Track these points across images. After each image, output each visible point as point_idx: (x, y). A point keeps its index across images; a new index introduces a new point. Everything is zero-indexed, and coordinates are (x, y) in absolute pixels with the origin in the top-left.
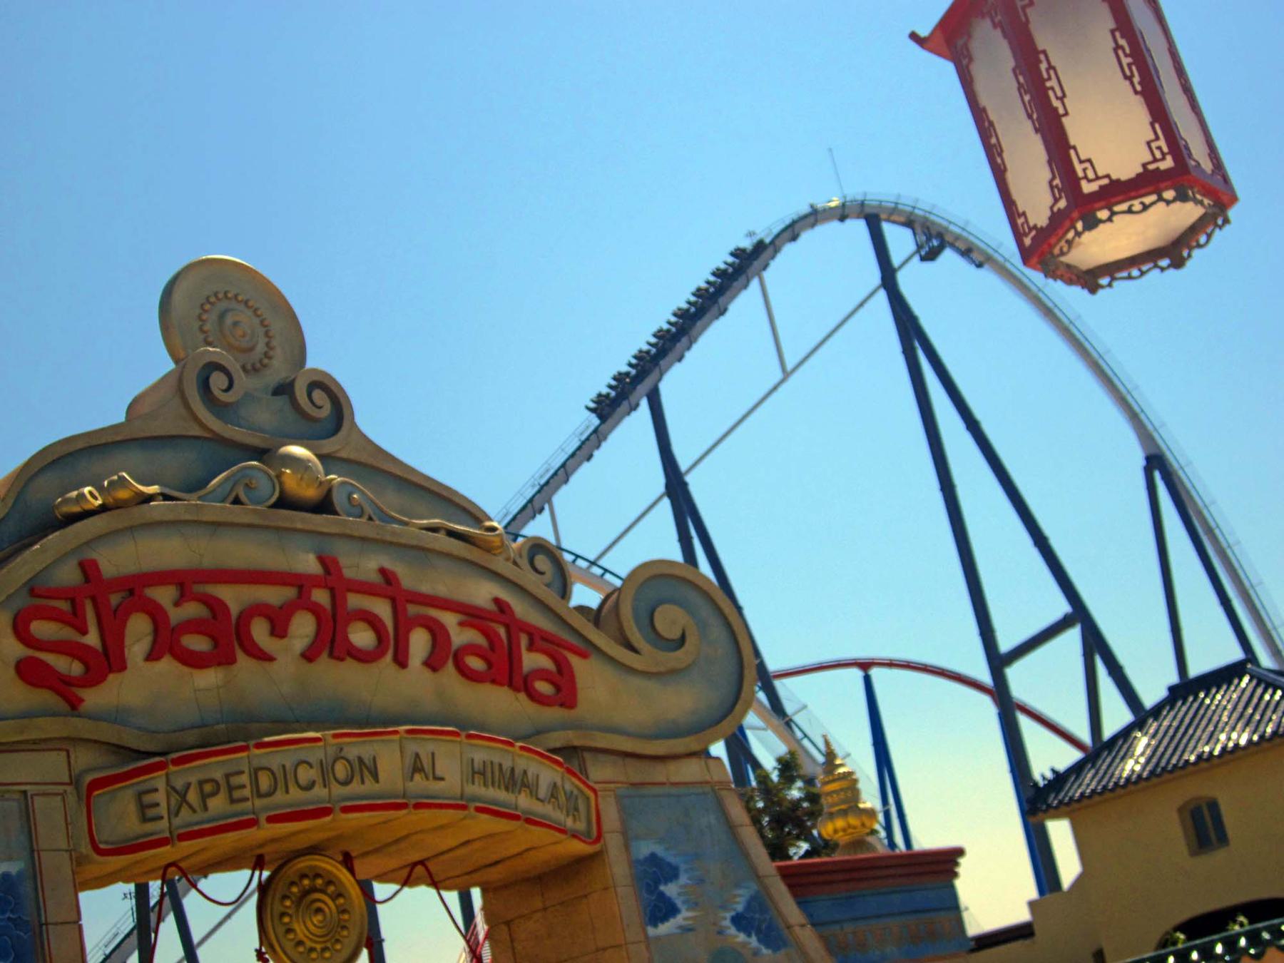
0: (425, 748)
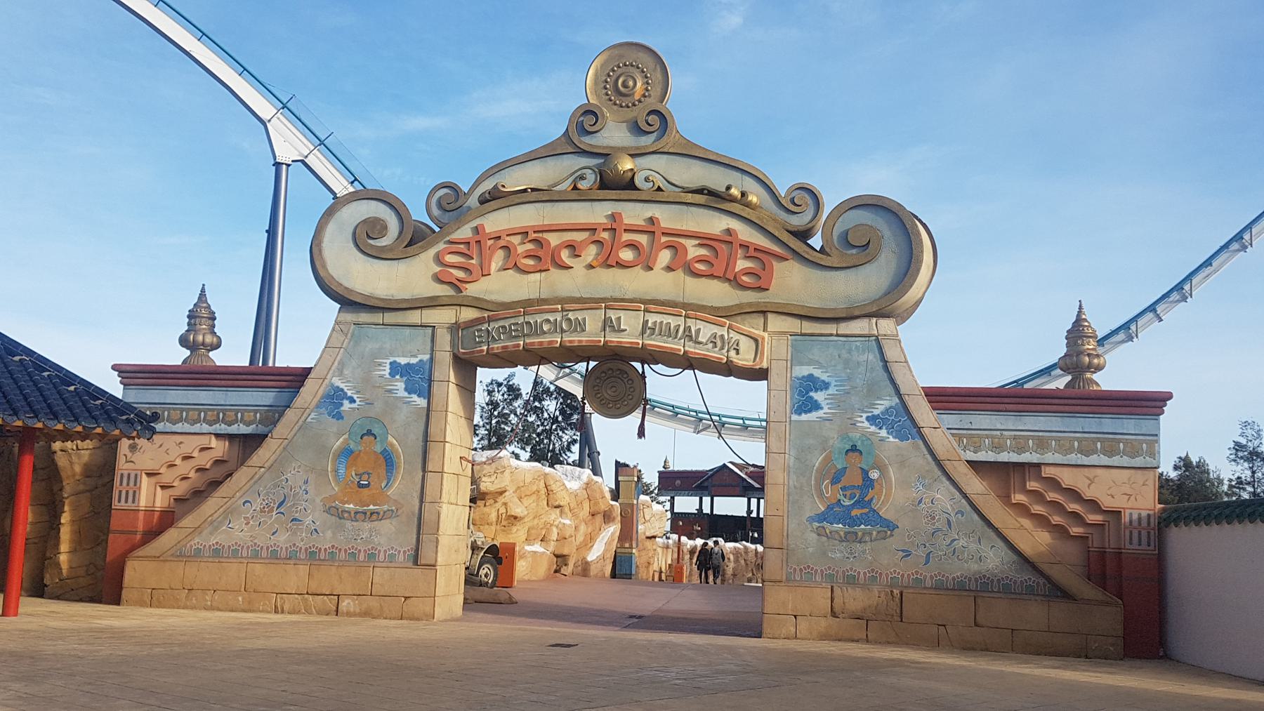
0: (613, 315)
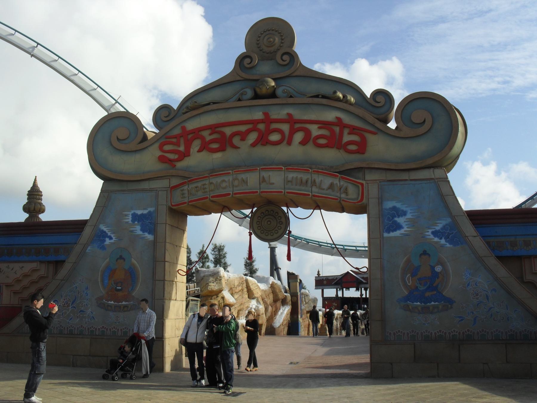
0: (265, 174)
